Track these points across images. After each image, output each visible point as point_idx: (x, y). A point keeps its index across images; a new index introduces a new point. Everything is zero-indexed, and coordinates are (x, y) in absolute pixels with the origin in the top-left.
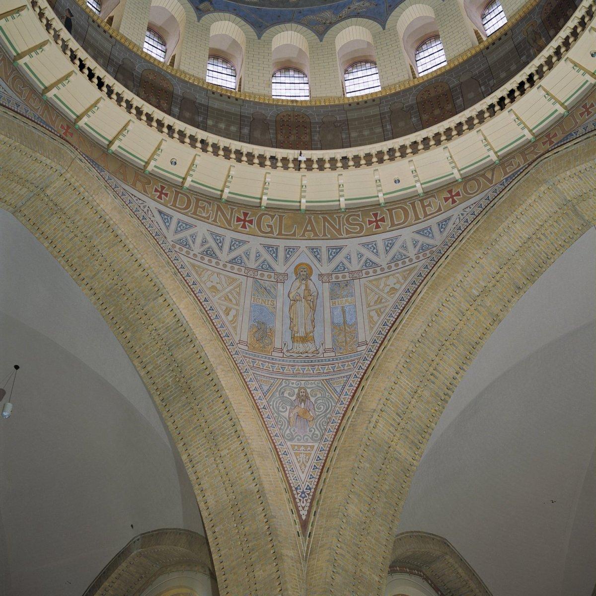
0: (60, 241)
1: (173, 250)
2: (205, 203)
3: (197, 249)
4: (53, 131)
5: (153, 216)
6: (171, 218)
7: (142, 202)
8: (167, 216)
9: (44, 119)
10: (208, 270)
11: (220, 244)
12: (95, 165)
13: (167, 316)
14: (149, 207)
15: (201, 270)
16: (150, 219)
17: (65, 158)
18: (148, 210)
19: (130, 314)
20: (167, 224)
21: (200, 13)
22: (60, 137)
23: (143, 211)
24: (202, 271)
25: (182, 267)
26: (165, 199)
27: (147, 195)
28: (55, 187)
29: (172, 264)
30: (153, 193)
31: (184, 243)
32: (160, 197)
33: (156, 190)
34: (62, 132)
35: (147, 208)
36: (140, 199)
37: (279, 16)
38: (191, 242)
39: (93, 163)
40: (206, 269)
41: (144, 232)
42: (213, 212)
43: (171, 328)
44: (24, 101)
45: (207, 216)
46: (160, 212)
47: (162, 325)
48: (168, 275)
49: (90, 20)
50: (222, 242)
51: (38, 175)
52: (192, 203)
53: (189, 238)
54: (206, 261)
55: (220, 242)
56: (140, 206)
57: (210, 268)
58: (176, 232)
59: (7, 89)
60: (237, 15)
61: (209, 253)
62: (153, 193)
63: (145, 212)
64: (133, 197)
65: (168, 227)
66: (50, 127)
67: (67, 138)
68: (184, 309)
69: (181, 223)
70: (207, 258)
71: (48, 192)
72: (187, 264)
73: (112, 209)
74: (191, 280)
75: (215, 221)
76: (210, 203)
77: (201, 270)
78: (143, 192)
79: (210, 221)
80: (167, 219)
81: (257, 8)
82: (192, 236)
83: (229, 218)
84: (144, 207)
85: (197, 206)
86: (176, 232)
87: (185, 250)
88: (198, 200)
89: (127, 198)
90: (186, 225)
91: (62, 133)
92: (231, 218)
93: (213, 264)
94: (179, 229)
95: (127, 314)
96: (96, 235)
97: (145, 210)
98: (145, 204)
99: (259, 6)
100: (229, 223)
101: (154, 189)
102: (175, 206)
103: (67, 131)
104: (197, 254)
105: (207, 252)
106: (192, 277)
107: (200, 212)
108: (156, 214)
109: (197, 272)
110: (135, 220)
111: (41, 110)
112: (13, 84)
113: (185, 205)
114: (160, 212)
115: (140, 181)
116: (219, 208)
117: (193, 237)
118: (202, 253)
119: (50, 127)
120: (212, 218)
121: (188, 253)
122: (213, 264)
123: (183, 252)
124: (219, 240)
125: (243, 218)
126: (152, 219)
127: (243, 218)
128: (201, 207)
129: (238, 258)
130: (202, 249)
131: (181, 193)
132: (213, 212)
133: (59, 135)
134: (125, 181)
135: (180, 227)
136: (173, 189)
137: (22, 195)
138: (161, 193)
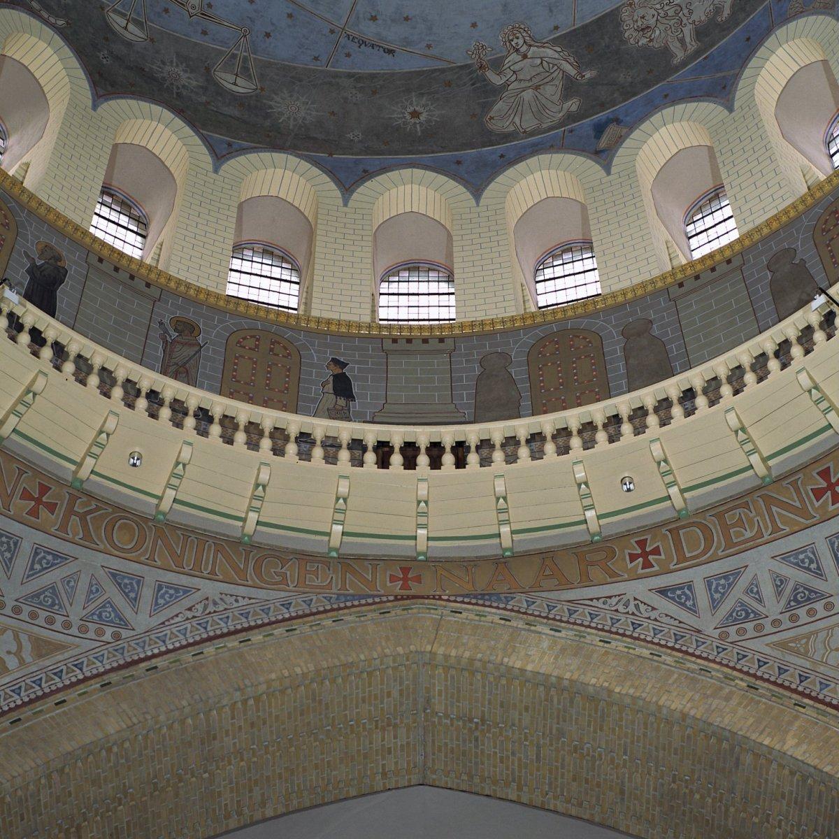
0: (526, 773)
1: (725, 645)
2: (738, 511)
3: (772, 607)
4: (377, 600)
5: (653, 609)
6: (690, 588)
7: (618, 598)
8: (679, 589)
9: (351, 592)
10: (816, 633)
11: (813, 566)
12: (490, 600)
13: (779, 779)
14: (635, 599)
15: (804, 641)
16: (649, 618)
17: (420, 631)
18: (637, 606)
19: (726, 819)
20: (689, 603)
21: (603, 157)
22: (396, 599)
23: (628, 613)
24: (807, 643)
25: (761, 664)
26: (824, 506)
27: (619, 579)
28: (440, 692)
29: (735, 673)
30: (630, 566)
31: (744, 614)
32: (647, 565)
33: (633, 558)
34: (397, 588)
35: (632, 603)
36: (610, 597)
37: (748, 39)
38: (755, 605)
39: (483, 598)
40: (812, 633)
41: (646, 653)
42: (762, 516)
43: (803, 798)
44: (297, 589)
45: (756, 530)
46: (663, 592)
47: (785, 802)
48: (734, 701)
49: (388, 345)
50: (815, 559)
51: (395, 694)
52: (714, 531)
53: (746, 599)
54: (804, 618)
55: (811, 562)
56: (617, 611)
57: (821, 624)
58: (715, 605)
59: (253, 592)
60: (674, 102)
61: (804, 597)
62: (630, 566)
63: (633, 614)
64: (595, 603)
65: (693, 610)
66: (370, 596)
67: (413, 592)
68: (798, 745)
69: (714, 583)
70: (802, 612)
71: (439, 707)
72: (767, 650)
73: (556, 658)
74: (792, 676)
75: (776, 529)
76: (746, 506)
77: (804, 641)
78: (609, 580)
79: (766, 537)
80: (684, 593)
81: (705, 58)
82: (748, 591)
83: (798, 504)
84: (626, 605)
85: (726, 528)
86: (715, 605)
87: (749, 626)
88: (720, 516)
89: (583, 614)
90: (726, 578)
91: (398, 591)
92: (802, 501)
93: (821, 613)
94: (717, 596)
95: (723, 823)
96: (565, 721)
97: (632, 608)
98: (625, 598)
99: (705, 50)
100: (803, 512)
101: (628, 557)
102: (686, 560)
103: (405, 579)
104: (779, 617)
105: (795, 600)
106: (792, 670)
107: (739, 534)
108: (657, 600)
109: (797, 653)
110: (618, 645)
111: (337, 583)
112: (262, 580)
113: (703, 542)
114: (663, 592)
115: (592, 564)
116: (769, 500)
117: (752, 592)
118: (788, 608)
119: (370, 596)
120: (767, 528)
121: (759, 628)
122: (821, 613)
123: (751, 633)
124: (806, 560)
125: (824, 485)
126: (654, 615)
127: (824, 485)
128: (734, 525)
129: (738, 609)
130: (783, 602)
131: (683, 527)
132: (762, 516)
133: (391, 598)
134: (567, 584)
135: (717, 591)
136: (663, 531)
137: (408, 743)
138: (645, 555)
